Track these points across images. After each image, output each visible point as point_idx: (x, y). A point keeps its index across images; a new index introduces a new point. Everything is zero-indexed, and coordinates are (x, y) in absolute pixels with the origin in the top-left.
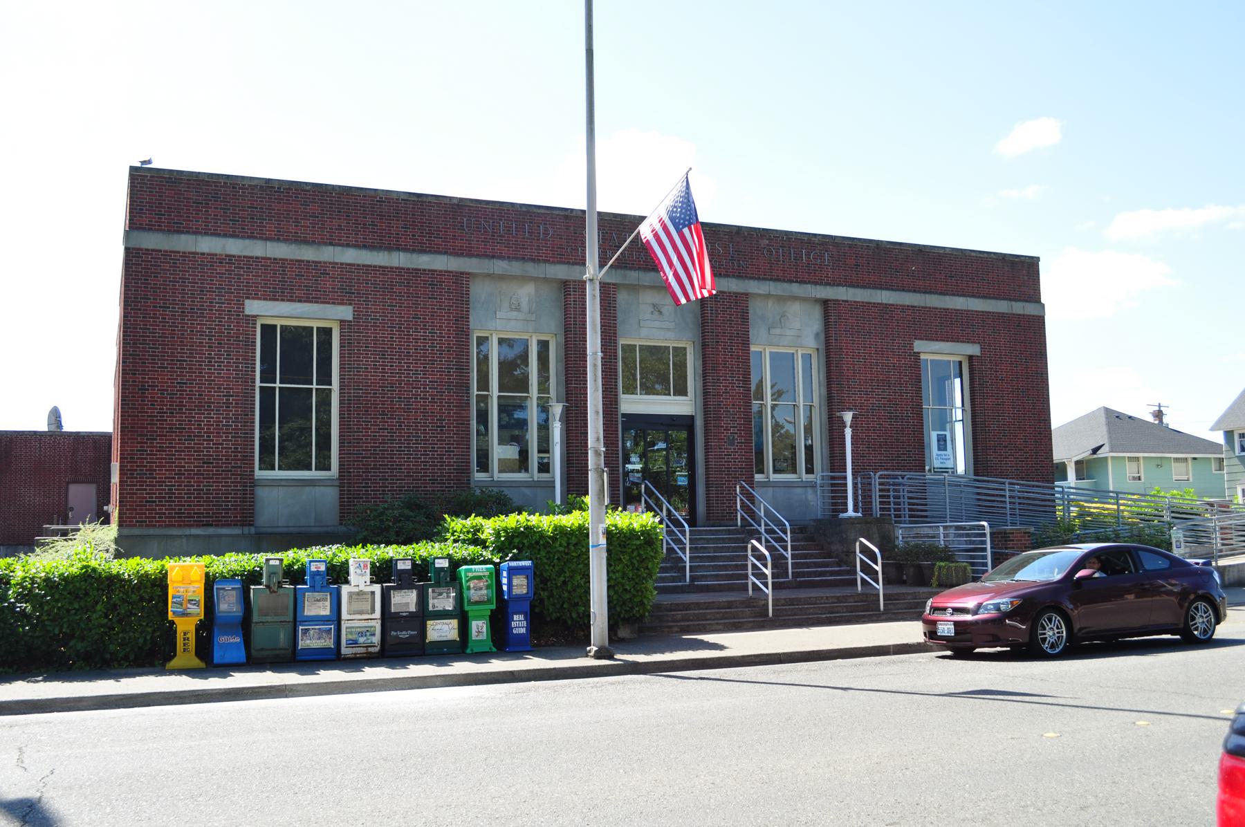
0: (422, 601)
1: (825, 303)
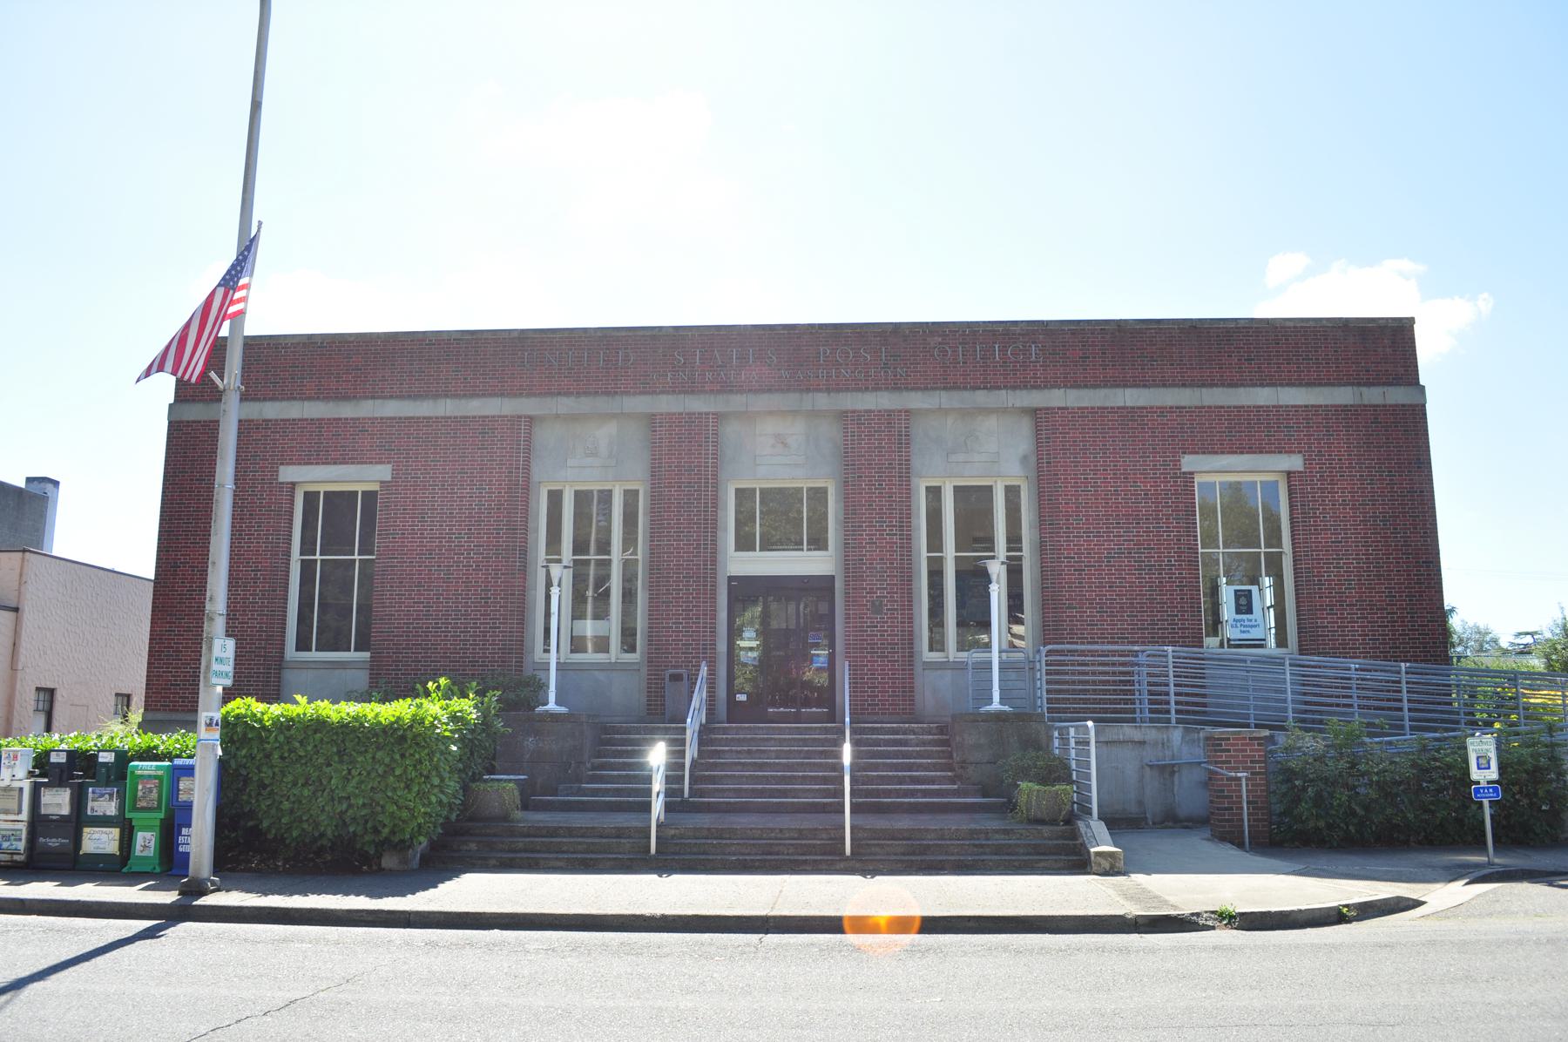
0: (79, 802)
1: (1034, 412)
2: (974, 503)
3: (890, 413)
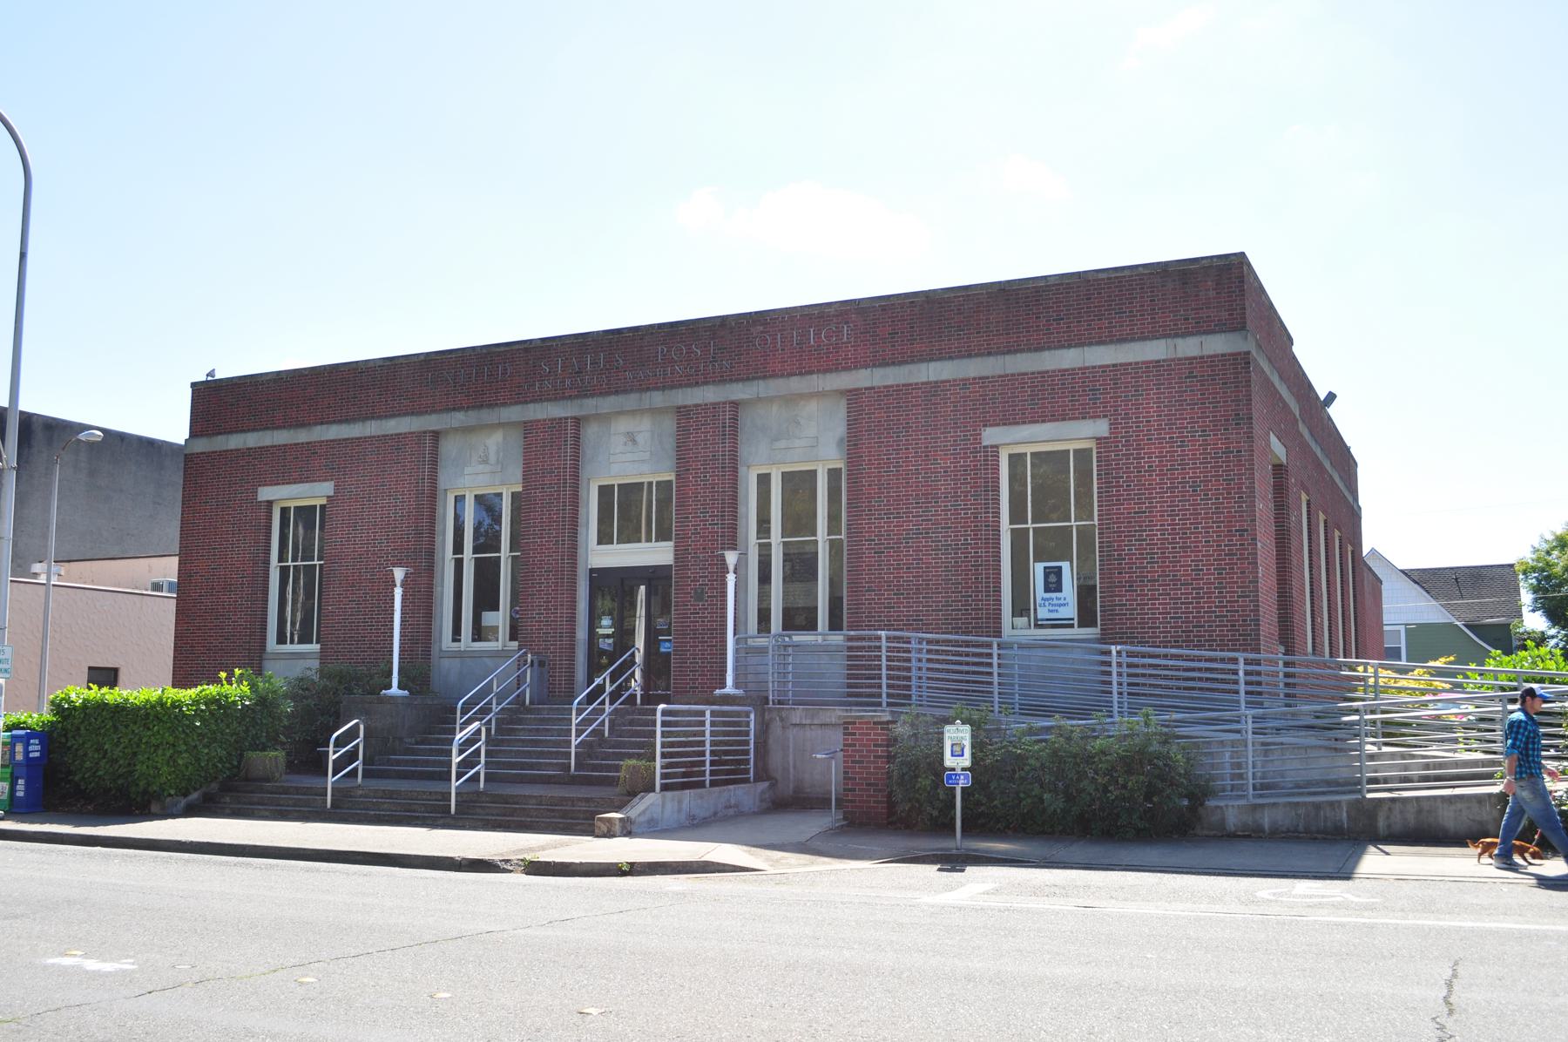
2: (487, 505)
3: (715, 405)
